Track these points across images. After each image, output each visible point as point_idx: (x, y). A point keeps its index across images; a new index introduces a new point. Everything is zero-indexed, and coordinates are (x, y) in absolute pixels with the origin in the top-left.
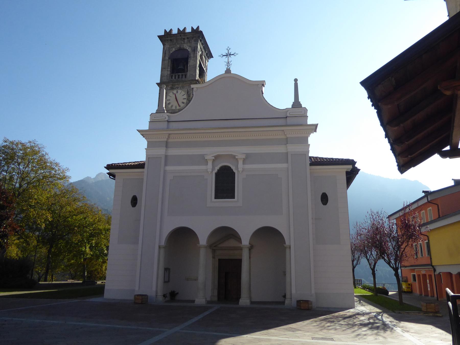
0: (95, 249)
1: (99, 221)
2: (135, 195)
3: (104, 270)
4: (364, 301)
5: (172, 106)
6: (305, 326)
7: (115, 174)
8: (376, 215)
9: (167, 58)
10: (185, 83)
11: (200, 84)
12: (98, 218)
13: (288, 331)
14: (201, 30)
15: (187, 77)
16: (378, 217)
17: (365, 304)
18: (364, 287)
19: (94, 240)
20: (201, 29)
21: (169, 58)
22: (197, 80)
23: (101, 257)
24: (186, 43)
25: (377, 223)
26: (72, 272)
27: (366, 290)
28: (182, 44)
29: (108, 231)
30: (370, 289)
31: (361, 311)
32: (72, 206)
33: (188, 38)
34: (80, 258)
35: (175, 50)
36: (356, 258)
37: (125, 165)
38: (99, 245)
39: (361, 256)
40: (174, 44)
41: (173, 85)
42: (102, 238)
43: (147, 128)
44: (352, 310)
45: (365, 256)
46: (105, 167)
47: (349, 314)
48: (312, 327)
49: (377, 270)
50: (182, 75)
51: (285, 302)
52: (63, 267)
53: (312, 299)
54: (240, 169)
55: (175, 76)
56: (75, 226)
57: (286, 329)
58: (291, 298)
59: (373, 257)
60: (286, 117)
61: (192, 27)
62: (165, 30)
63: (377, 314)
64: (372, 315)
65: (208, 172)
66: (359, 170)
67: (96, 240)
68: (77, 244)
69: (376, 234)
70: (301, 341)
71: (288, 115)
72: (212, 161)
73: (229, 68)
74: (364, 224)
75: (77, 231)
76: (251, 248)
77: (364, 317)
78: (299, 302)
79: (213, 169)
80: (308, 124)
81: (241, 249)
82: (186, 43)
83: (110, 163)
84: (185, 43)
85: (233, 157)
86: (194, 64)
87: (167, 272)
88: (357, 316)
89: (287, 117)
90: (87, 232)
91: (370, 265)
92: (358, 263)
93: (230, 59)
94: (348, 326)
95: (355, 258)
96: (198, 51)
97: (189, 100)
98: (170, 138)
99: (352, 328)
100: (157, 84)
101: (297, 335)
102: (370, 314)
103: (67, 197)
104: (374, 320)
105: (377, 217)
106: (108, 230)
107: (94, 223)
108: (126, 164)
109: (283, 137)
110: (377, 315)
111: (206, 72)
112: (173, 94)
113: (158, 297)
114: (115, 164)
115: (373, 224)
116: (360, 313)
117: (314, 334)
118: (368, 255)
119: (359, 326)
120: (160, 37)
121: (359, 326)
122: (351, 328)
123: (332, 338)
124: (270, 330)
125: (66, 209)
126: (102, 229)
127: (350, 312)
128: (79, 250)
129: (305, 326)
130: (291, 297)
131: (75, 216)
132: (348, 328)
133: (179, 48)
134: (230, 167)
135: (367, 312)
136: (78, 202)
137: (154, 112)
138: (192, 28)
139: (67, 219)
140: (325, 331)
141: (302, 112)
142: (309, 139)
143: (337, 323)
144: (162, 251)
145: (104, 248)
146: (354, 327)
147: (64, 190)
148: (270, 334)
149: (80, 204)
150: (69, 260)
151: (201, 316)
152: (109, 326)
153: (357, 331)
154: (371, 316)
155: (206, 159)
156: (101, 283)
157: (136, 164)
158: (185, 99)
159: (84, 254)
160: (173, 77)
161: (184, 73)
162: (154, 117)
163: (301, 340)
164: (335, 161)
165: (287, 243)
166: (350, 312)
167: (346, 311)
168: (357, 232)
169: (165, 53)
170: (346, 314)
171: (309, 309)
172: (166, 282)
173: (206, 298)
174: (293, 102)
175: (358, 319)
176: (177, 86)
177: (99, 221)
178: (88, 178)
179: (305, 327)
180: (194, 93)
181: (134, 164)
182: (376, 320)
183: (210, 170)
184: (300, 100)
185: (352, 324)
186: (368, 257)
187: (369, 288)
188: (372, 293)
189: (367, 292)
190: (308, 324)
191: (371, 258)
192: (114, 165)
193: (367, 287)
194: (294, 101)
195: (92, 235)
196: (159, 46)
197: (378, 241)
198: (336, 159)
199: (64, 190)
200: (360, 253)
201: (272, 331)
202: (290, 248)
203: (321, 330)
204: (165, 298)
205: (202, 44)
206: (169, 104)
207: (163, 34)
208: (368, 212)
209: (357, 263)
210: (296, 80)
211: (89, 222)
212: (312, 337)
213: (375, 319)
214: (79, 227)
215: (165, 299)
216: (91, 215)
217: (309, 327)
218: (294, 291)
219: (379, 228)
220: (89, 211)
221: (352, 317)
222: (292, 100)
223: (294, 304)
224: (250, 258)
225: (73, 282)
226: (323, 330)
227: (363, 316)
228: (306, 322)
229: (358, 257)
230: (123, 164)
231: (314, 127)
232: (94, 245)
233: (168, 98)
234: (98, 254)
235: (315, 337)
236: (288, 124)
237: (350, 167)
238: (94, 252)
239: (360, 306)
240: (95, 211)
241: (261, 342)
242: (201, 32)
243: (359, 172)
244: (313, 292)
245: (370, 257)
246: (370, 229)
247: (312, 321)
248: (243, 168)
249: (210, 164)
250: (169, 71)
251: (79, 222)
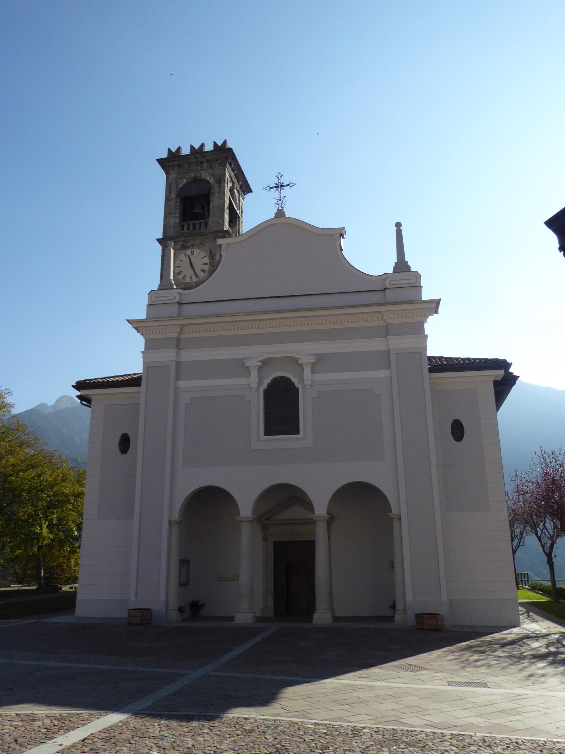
0: (58, 529)
1: (64, 480)
2: (125, 432)
3: (72, 565)
4: (536, 613)
5: (184, 277)
6: (433, 660)
7: (91, 396)
8: (551, 456)
9: (173, 196)
11: (231, 237)
12: (61, 475)
13: (404, 671)
14: (231, 147)
15: (208, 225)
16: (554, 461)
17: (538, 619)
18: (534, 586)
19: (56, 513)
20: (229, 145)
21: (176, 195)
22: (226, 231)
23: (68, 543)
24: (205, 169)
25: (553, 472)
26: (19, 571)
27: (537, 593)
28: (198, 170)
29: (79, 497)
30: (544, 591)
31: (533, 631)
32: (18, 455)
33: (208, 161)
34: (32, 546)
35: (186, 183)
36: (516, 535)
37: (108, 381)
38: (65, 522)
39: (525, 532)
41: (184, 241)
42: (70, 510)
43: (143, 315)
44: (515, 630)
45: (534, 532)
46: (73, 386)
47: (510, 637)
48: (447, 663)
49: (555, 556)
50: (200, 224)
51: (394, 616)
52: (3, 563)
53: (442, 611)
54: (307, 382)
55: (189, 226)
56: (23, 490)
57: (401, 667)
58: (405, 610)
59: (548, 532)
60: (383, 289)
61: (215, 142)
63: (561, 636)
64: (553, 638)
65: (251, 389)
66: (516, 378)
67: (59, 514)
68: (26, 521)
69: (553, 492)
70: (428, 689)
71: (388, 285)
72: (257, 370)
73: (282, 208)
74: (530, 474)
75: (25, 498)
76: (330, 520)
77: (539, 642)
78: (419, 616)
79: (260, 383)
80: (423, 299)
81: (312, 522)
82: (205, 169)
83: (82, 378)
84: (204, 170)
85: (295, 361)
86: (220, 204)
87: (183, 567)
88: (525, 641)
89: (385, 289)
90: (44, 499)
91: (543, 547)
92: (521, 543)
93: (283, 193)
94: (511, 659)
95: (515, 535)
96: (226, 183)
97: (214, 266)
98: (184, 332)
99: (518, 663)
100: (158, 240)
101: (420, 677)
102: (548, 637)
103: (7, 440)
104: (557, 648)
105: (552, 461)
106: (80, 495)
107: (54, 483)
108: (108, 379)
109: (382, 324)
110: (561, 638)
111: (241, 217)
112: (186, 256)
113: (170, 612)
114: (90, 380)
115: (546, 473)
116: (531, 635)
117: (451, 676)
118: (538, 529)
119: (530, 659)
120: (160, 161)
121: (531, 660)
122: (516, 664)
123: (484, 682)
124: (372, 668)
125: (7, 461)
126: (69, 494)
127: (511, 634)
128: (30, 531)
129: (433, 660)
130: (405, 608)
131: (23, 472)
132: (511, 663)
133: (193, 178)
134: (290, 379)
135: (542, 634)
136: (26, 448)
137: (156, 287)
138: (215, 144)
139: (8, 478)
140: (470, 669)
141: (411, 279)
142: (426, 325)
143: (490, 654)
144: (175, 530)
145: (73, 528)
146: (523, 661)
147: (3, 429)
148: (371, 677)
149: (30, 451)
150: (13, 550)
151: (246, 646)
152: (87, 666)
153: (528, 669)
154: (551, 640)
155: (248, 367)
156: (68, 588)
157: (127, 379)
158: (207, 264)
159: (38, 539)
160: (185, 228)
161: (203, 221)
162: (156, 297)
163: (429, 688)
164: (473, 363)
165: (395, 511)
166: (511, 634)
167: (504, 632)
168: (518, 488)
169: (170, 188)
170: (507, 638)
171: (439, 629)
172: (183, 584)
173: (254, 613)
174: (395, 263)
175: (528, 647)
177: (64, 480)
178: (43, 405)
179: (435, 664)
180: (223, 254)
181: (123, 379)
182: (561, 647)
183: (254, 385)
184: (408, 258)
185: (519, 655)
186: (539, 532)
187: (543, 588)
188: (548, 597)
189: (540, 595)
190: (438, 657)
191: (545, 534)
192: (88, 381)
193: (539, 587)
194: (396, 262)
195: (51, 506)
196: (160, 176)
197: (556, 502)
198: (475, 359)
199: (3, 429)
200: (524, 525)
201: (375, 670)
202: (400, 519)
203: (463, 668)
204: (182, 613)
205: (232, 170)
206: (179, 273)
207: (166, 156)
208: (535, 453)
209: (519, 544)
210: (398, 225)
211: (46, 483)
212: (448, 682)
213: (559, 645)
214: (29, 491)
215: (182, 615)
216: (49, 470)
217: (441, 663)
218: (409, 597)
219: (557, 480)
220: (46, 463)
221: (517, 644)
222: (393, 259)
223: (411, 621)
224: (329, 537)
225: (20, 589)
226: (467, 667)
227: (537, 640)
228: (436, 654)
229: (521, 532)
230: (103, 380)
231: (434, 305)
232: (55, 522)
233: (177, 262)
234: (63, 537)
235: (454, 681)
236: (388, 301)
237: (501, 373)
238: (56, 534)
239: (529, 621)
240: (56, 463)
241: (357, 691)
242: (231, 150)
243: (516, 382)
244: (444, 598)
245: (542, 532)
246: (540, 482)
247: (445, 652)
248: (311, 381)
249: (254, 374)
251: (29, 483)
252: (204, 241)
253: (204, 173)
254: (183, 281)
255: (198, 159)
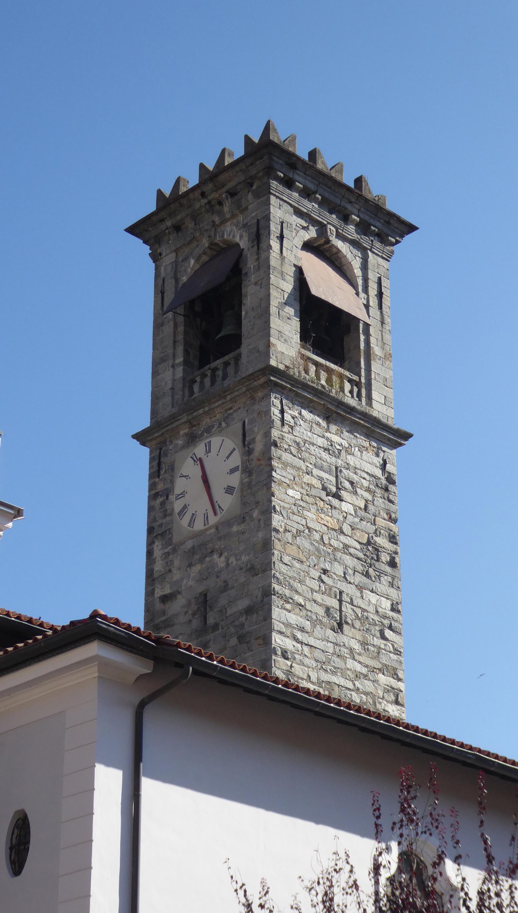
10: (229, 397)
24: (228, 216)
33: (232, 194)
35: (198, 266)
40: (188, 240)
62: (202, 167)
169: (163, 293)
176: (208, 420)
250: (179, 365)
252: (231, 408)
253: (228, 229)
254: (191, 529)
255: (210, 198)
